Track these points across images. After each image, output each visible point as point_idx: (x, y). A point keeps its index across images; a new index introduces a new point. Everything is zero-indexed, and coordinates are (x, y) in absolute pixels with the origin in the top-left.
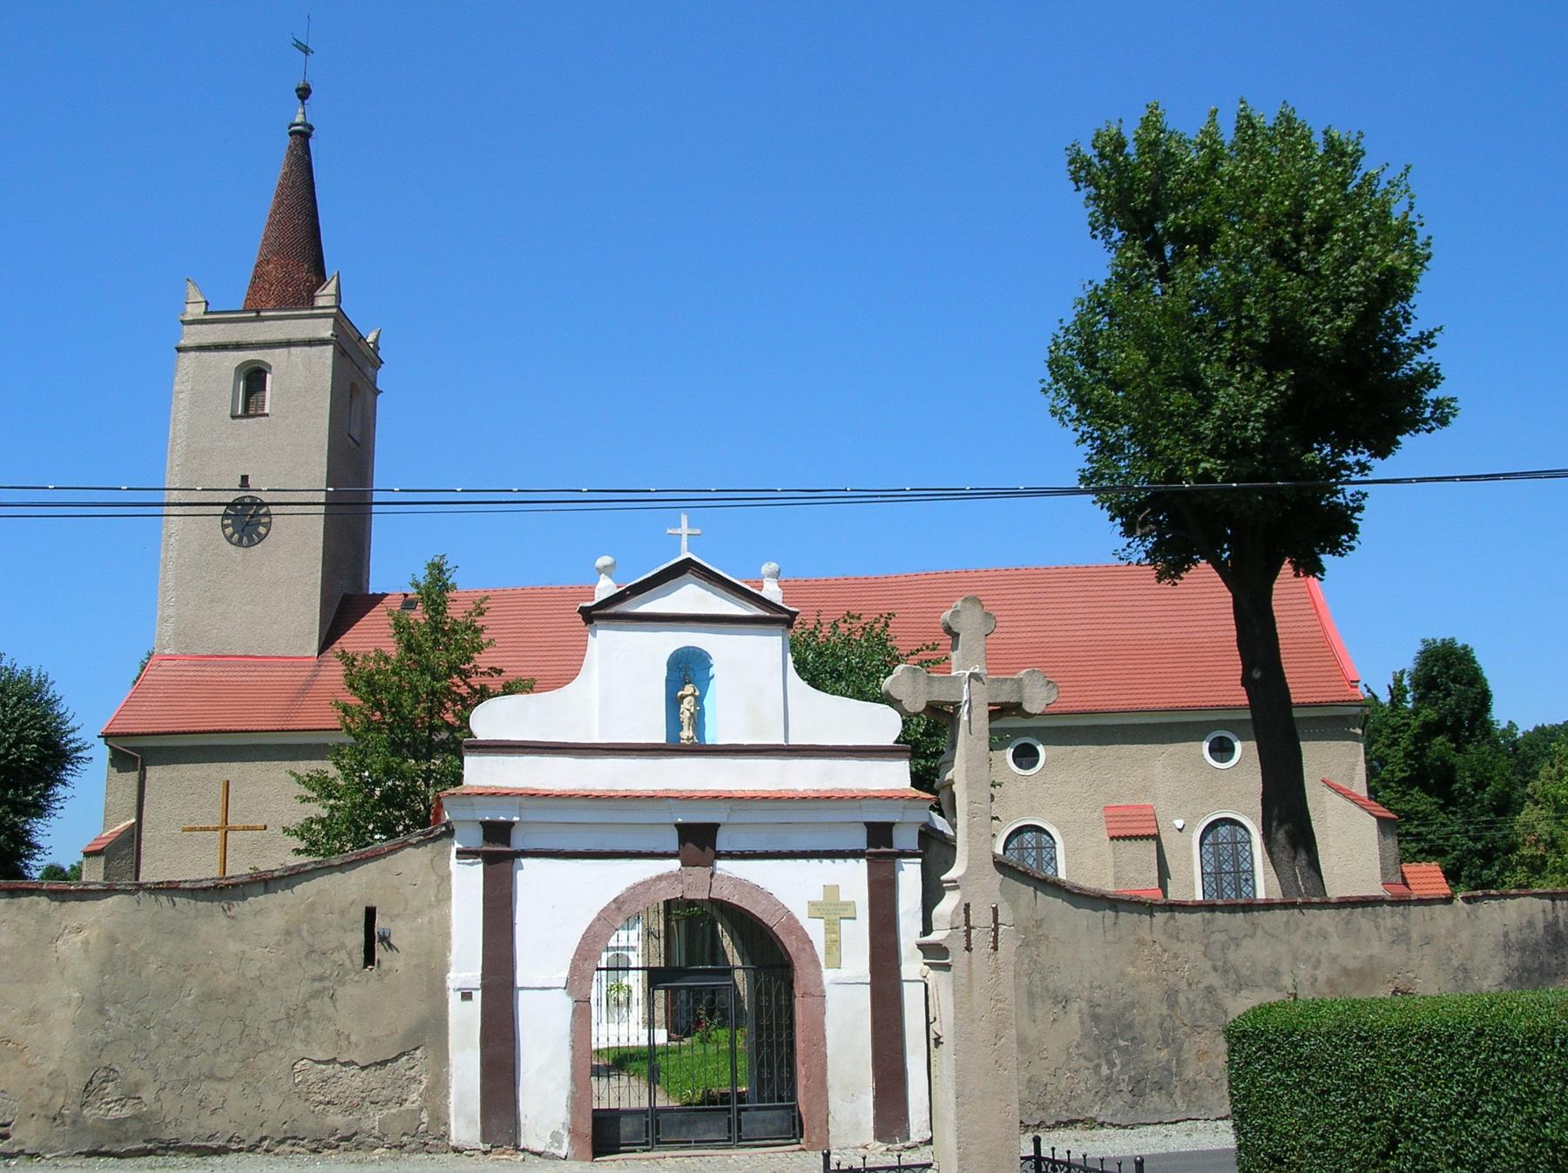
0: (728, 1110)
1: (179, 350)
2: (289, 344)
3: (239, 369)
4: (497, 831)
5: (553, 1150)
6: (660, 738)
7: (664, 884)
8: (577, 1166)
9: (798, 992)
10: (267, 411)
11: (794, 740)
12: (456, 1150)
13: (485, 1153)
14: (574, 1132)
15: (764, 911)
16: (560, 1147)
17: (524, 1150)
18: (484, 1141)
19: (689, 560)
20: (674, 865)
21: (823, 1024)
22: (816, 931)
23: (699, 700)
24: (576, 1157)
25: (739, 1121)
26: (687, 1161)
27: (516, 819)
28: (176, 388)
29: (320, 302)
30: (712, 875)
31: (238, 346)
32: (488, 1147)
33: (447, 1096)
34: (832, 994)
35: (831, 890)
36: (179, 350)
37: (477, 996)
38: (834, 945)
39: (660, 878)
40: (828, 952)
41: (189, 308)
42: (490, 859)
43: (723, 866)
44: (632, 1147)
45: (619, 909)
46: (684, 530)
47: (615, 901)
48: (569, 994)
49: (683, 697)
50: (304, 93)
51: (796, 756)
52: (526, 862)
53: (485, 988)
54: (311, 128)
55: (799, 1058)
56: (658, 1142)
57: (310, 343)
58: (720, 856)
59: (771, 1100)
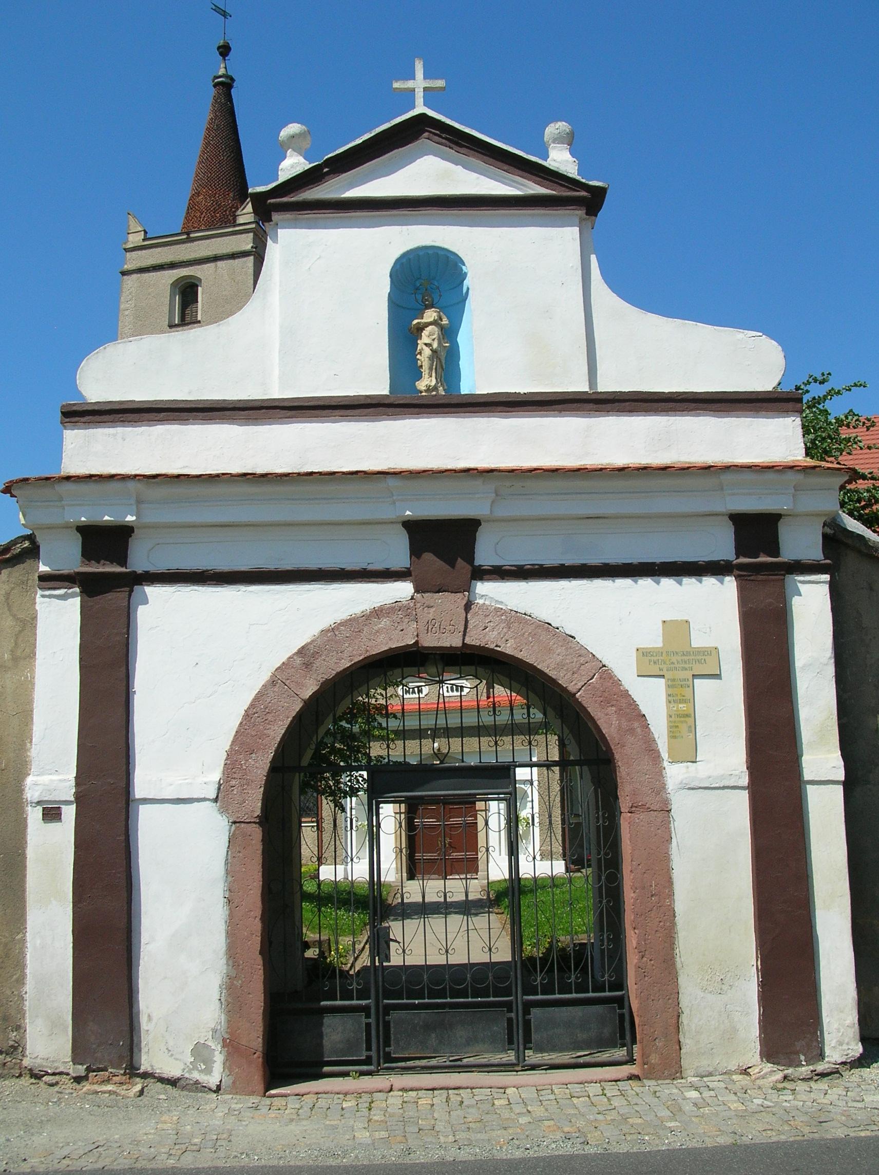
0: (509, 1006)
1: (124, 273)
2: (216, 259)
3: (174, 285)
4: (105, 541)
5: (196, 1076)
6: (380, 386)
7: (385, 622)
8: (240, 1103)
9: (624, 803)
10: (199, 319)
11: (607, 384)
12: (36, 1075)
13: (78, 1080)
14: (231, 1045)
15: (560, 666)
16: (208, 1071)
17: (145, 1075)
18: (76, 1060)
19: (423, 116)
20: (403, 590)
21: (665, 859)
22: (651, 697)
23: (449, 333)
24: (235, 1089)
25: (527, 1024)
26: (425, 1100)
27: (130, 518)
28: (122, 306)
29: (241, 220)
30: (468, 607)
31: (172, 266)
32: (81, 1070)
33: (21, 981)
34: (684, 808)
35: (676, 630)
36: (124, 273)
37: (69, 813)
38: (683, 721)
39: (378, 613)
40: (673, 733)
41: (131, 237)
42: (90, 586)
43: (488, 592)
44: (345, 1065)
45: (307, 665)
46: (419, 83)
47: (301, 652)
48: (224, 810)
49: (420, 329)
50: (225, 51)
51: (608, 412)
52: (152, 591)
53: (80, 799)
54: (232, 80)
55: (629, 917)
56: (389, 1059)
57: (233, 256)
58: (481, 574)
59: (582, 988)
